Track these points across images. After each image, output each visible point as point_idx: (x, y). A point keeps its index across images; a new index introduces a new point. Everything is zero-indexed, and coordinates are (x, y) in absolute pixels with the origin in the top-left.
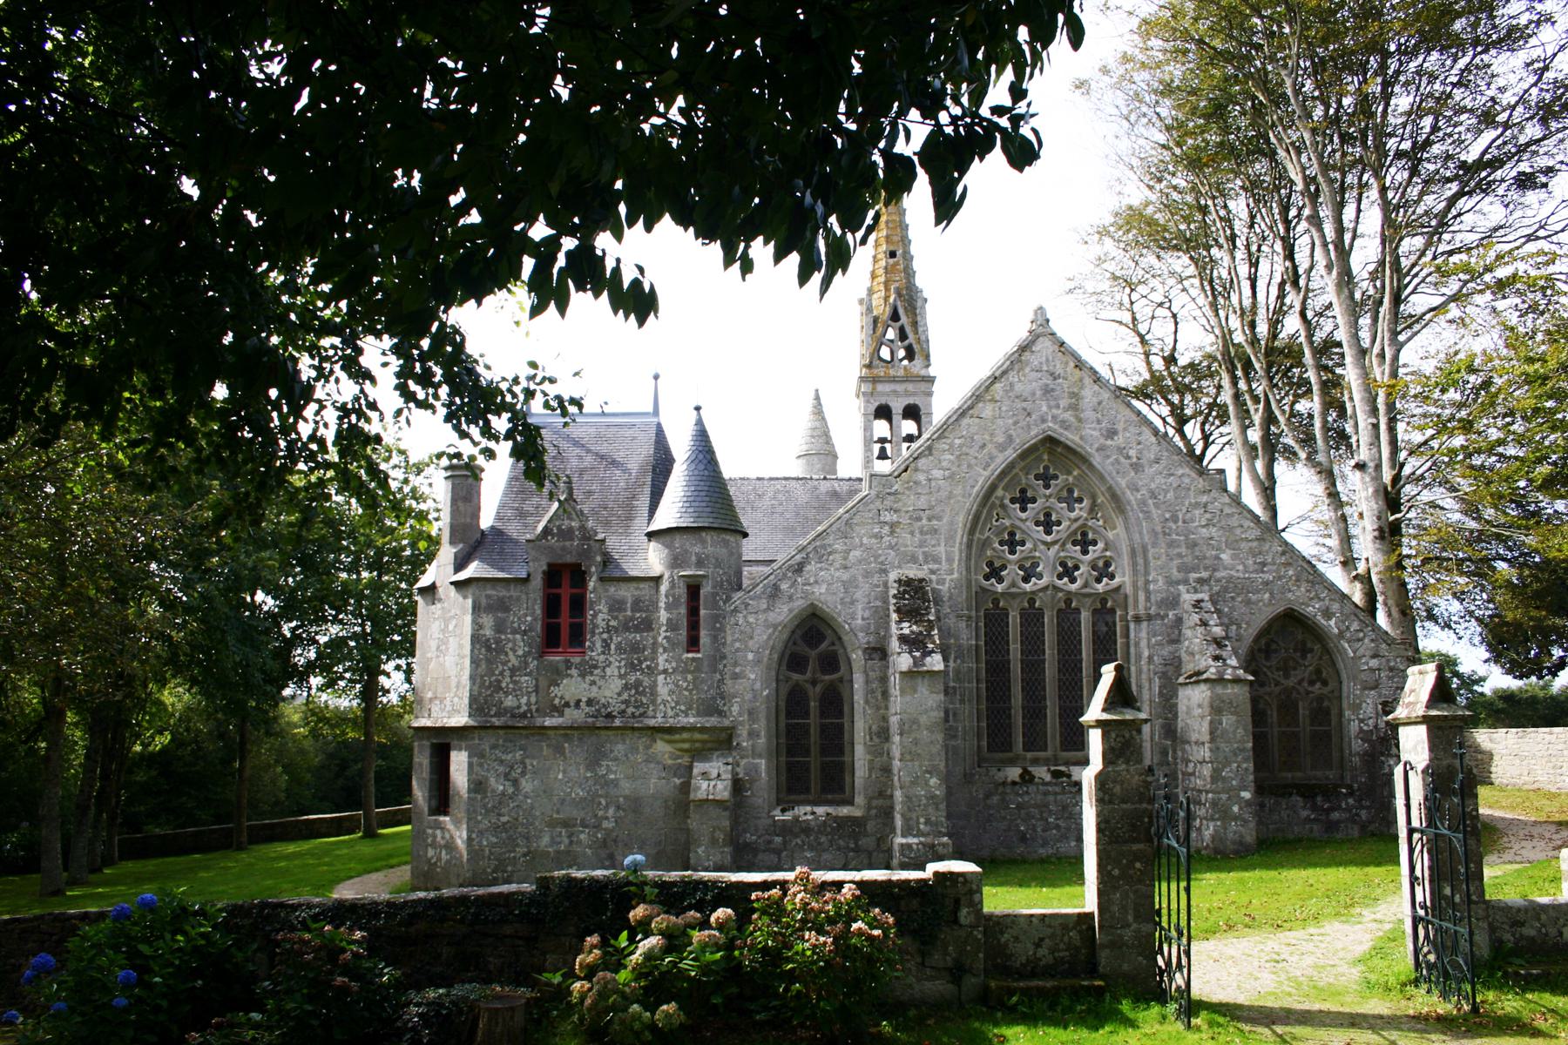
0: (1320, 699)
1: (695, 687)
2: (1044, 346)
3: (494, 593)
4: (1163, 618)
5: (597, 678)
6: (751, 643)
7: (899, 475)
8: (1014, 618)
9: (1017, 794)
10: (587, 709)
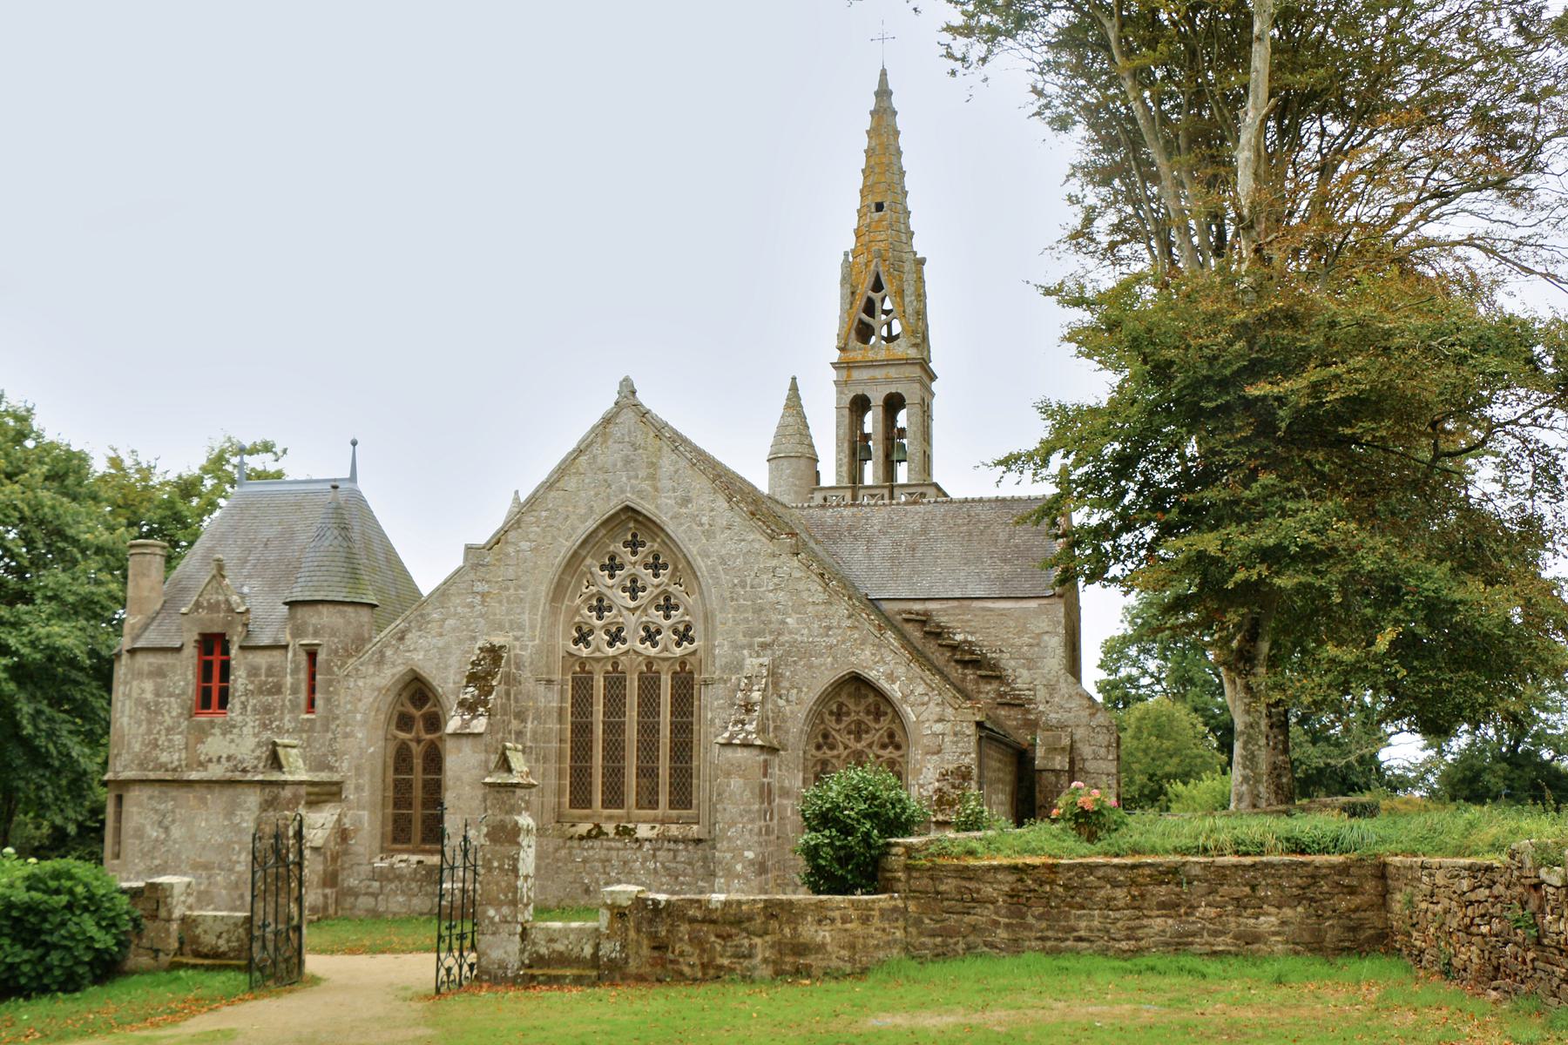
1: (309, 745)
2: (628, 417)
4: (725, 682)
6: (360, 705)
8: (599, 682)
9: (584, 849)
10: (227, 765)
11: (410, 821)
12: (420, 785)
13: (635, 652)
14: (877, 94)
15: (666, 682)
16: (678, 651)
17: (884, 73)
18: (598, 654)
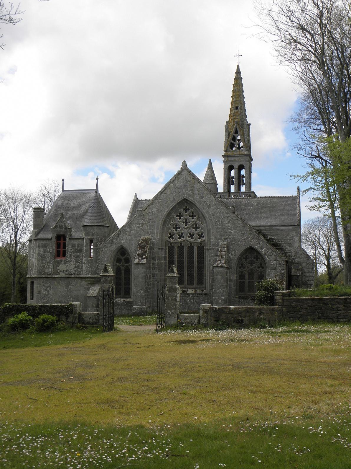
0: (261, 272)
2: (185, 173)
3: (43, 242)
4: (214, 249)
5: (68, 265)
7: (145, 210)
8: (176, 249)
10: (66, 273)
11: (121, 289)
12: (124, 278)
13: (187, 240)
14: (236, 73)
15: (196, 249)
16: (199, 240)
17: (238, 67)
18: (176, 241)
